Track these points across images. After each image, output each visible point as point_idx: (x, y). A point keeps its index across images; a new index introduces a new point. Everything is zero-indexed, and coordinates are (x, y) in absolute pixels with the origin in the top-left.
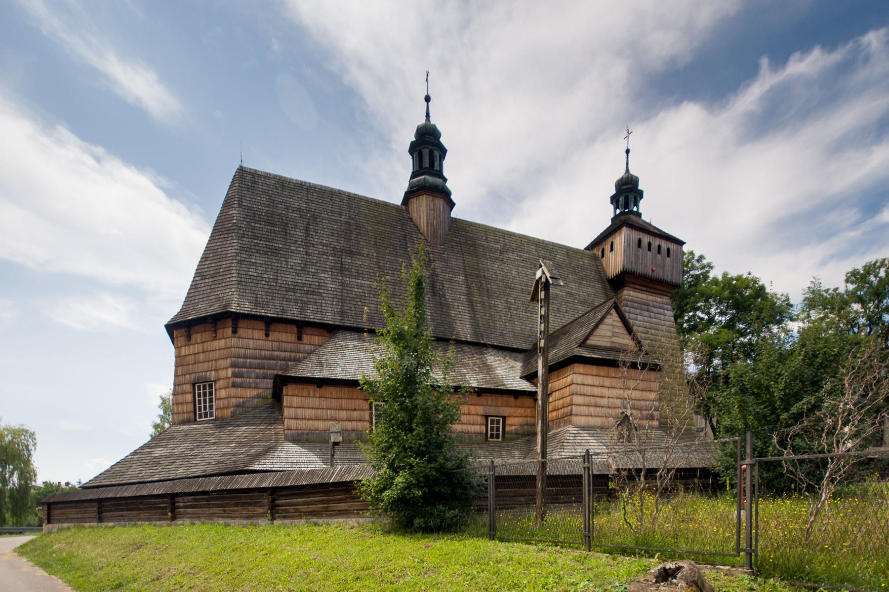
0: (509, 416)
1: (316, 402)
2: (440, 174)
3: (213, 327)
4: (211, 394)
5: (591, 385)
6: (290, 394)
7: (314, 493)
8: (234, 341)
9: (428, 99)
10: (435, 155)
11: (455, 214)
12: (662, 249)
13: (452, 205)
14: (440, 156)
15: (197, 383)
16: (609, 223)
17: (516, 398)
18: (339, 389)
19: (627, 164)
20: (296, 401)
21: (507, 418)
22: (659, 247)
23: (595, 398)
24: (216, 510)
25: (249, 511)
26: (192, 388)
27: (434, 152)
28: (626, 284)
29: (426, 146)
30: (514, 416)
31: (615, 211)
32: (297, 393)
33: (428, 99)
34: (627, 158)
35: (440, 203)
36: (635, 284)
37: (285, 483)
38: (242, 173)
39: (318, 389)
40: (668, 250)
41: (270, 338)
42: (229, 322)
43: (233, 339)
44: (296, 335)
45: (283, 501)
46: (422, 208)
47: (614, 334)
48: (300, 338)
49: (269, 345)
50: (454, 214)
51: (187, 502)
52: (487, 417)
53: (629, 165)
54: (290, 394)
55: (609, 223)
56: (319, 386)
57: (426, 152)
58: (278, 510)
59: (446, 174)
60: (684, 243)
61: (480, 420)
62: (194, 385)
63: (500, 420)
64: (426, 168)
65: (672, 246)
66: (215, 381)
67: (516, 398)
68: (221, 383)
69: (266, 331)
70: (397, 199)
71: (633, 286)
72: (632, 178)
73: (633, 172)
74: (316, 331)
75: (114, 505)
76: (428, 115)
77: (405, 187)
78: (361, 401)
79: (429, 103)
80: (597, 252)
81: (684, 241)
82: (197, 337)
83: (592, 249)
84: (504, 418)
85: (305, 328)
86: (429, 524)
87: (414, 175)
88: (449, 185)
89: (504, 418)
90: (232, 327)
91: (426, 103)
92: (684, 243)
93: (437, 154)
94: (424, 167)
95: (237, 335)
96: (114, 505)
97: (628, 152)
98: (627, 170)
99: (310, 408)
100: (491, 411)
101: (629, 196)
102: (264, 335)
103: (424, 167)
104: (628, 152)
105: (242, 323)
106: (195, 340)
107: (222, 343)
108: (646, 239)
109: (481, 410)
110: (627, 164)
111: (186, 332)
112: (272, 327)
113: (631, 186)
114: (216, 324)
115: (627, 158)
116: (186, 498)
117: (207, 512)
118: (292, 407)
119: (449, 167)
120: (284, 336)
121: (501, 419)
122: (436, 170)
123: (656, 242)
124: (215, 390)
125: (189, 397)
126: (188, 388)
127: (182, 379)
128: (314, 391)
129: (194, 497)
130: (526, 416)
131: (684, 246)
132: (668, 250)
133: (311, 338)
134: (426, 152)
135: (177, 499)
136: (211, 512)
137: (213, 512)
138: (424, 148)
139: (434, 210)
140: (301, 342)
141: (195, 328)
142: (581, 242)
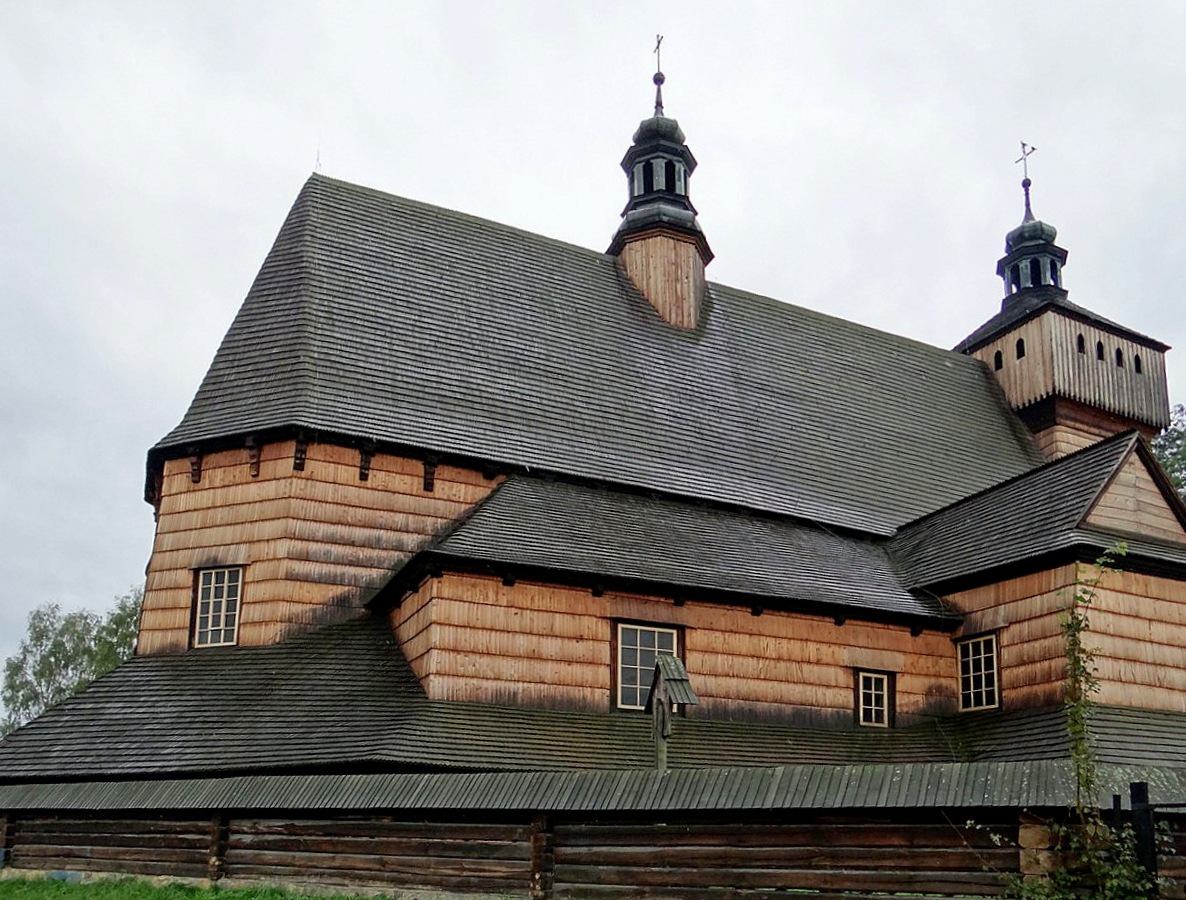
0: (903, 673)
1: (498, 616)
2: (683, 201)
3: (252, 457)
4: (232, 591)
5: (1113, 613)
6: (446, 594)
7: (693, 834)
8: (297, 486)
9: (659, 79)
10: (677, 169)
11: (714, 273)
12: (1125, 357)
13: (707, 255)
14: (685, 171)
15: (204, 569)
16: (998, 310)
17: (915, 633)
18: (546, 591)
19: (1028, 205)
20: (459, 612)
21: (898, 676)
22: (1119, 353)
23: (1126, 641)
24: (359, 860)
25: (465, 869)
26: (191, 578)
27: (674, 166)
28: (1058, 420)
29: (661, 154)
30: (912, 674)
31: (1009, 289)
32: (460, 593)
33: (659, 79)
34: (1027, 194)
35: (689, 251)
36: (1076, 420)
37: (572, 799)
38: (1067, 252)
39: (506, 589)
40: (1137, 360)
41: (369, 483)
42: (290, 448)
43: (295, 480)
44: (422, 480)
45: (584, 850)
46: (652, 261)
47: (1140, 507)
48: (429, 486)
49: (367, 496)
50: (714, 273)
51: (264, 833)
52: (856, 671)
53: (1032, 207)
54: (446, 595)
55: (996, 309)
56: (508, 583)
57: (659, 166)
58: (21, 825)
59: (695, 198)
60: (1168, 348)
61: (844, 678)
62: (196, 572)
63: (882, 680)
64: (659, 191)
65: (1146, 354)
66: (244, 566)
67: (915, 633)
68: (253, 573)
69: (361, 468)
70: (601, 244)
71: (1072, 424)
72: (1042, 230)
73: (1039, 216)
74: (464, 474)
75: (49, 829)
76: (659, 105)
77: (616, 223)
78: (595, 619)
79: (662, 87)
80: (986, 355)
81: (1166, 343)
82: (214, 475)
83: (972, 353)
84: (892, 676)
85: (440, 467)
86: (217, 863)
87: (634, 203)
88: (703, 223)
89: (892, 676)
90: (297, 458)
91: (655, 87)
92: (1168, 348)
93: (680, 167)
94: (655, 189)
95: (303, 474)
96: (49, 829)
97: (1026, 184)
98: (1029, 214)
99: (487, 629)
100: (865, 658)
101: (1041, 260)
102: (358, 476)
103: (655, 189)
104: (1026, 184)
105: (315, 451)
106: (210, 482)
107: (270, 489)
108: (1093, 336)
109: (845, 655)
110: (1028, 205)
111: (193, 464)
112: (375, 462)
113: (1042, 242)
114: (260, 450)
115: (1027, 194)
116: (263, 825)
117: (326, 864)
118: (450, 625)
119: (699, 188)
120: (399, 482)
121: (885, 677)
122: (680, 196)
123: (1113, 343)
124: (244, 584)
125: (185, 597)
126: (185, 577)
127: (168, 559)
128: (497, 594)
129: (289, 822)
130: (937, 676)
131: (1167, 353)
132: (1137, 360)
133: (452, 488)
134: (659, 166)
135: (235, 825)
136: (337, 863)
137: (349, 863)
138: (658, 157)
139: (676, 264)
140: (430, 494)
141: (212, 459)
142: (948, 335)
